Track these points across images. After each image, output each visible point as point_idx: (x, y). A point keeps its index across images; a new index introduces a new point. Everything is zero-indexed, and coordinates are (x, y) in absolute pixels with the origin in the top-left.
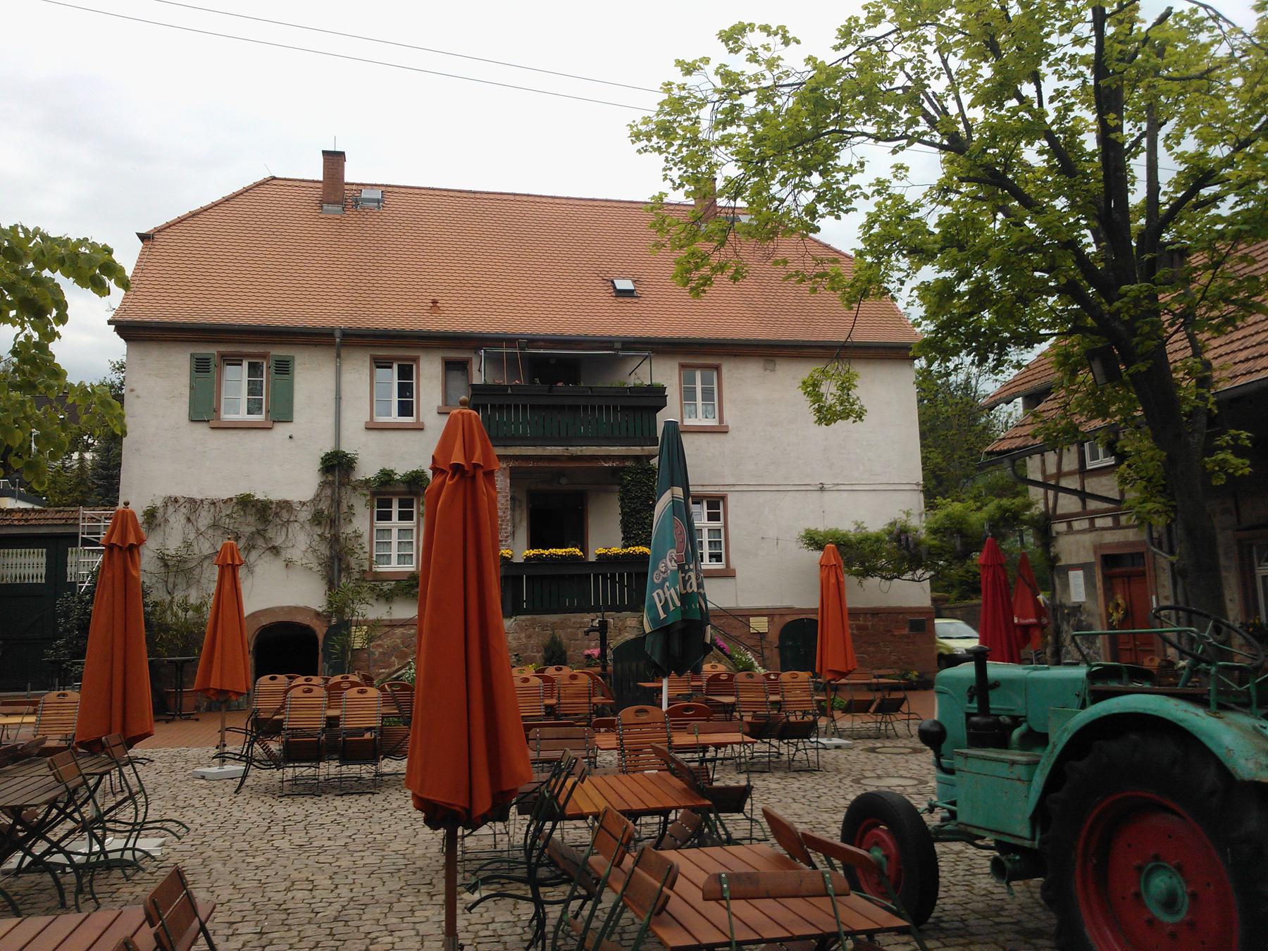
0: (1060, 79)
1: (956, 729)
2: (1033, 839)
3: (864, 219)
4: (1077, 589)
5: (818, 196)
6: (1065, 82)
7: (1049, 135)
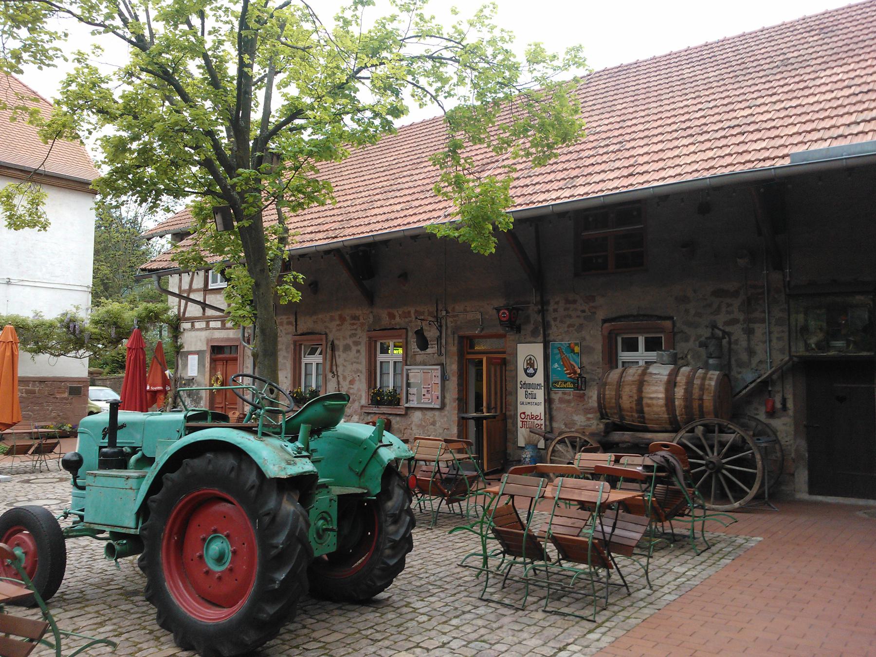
0: (217, 21)
1: (91, 458)
2: (137, 528)
3: (64, 78)
4: (192, 367)
5: (25, 46)
6: (220, 24)
7: (205, 57)
